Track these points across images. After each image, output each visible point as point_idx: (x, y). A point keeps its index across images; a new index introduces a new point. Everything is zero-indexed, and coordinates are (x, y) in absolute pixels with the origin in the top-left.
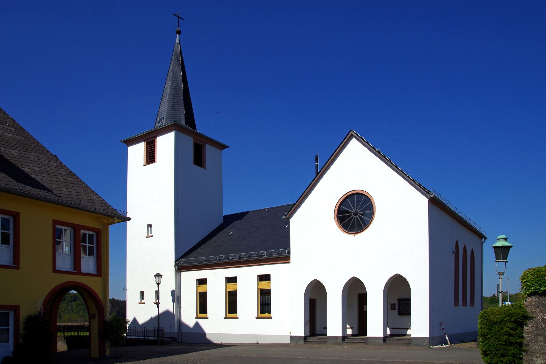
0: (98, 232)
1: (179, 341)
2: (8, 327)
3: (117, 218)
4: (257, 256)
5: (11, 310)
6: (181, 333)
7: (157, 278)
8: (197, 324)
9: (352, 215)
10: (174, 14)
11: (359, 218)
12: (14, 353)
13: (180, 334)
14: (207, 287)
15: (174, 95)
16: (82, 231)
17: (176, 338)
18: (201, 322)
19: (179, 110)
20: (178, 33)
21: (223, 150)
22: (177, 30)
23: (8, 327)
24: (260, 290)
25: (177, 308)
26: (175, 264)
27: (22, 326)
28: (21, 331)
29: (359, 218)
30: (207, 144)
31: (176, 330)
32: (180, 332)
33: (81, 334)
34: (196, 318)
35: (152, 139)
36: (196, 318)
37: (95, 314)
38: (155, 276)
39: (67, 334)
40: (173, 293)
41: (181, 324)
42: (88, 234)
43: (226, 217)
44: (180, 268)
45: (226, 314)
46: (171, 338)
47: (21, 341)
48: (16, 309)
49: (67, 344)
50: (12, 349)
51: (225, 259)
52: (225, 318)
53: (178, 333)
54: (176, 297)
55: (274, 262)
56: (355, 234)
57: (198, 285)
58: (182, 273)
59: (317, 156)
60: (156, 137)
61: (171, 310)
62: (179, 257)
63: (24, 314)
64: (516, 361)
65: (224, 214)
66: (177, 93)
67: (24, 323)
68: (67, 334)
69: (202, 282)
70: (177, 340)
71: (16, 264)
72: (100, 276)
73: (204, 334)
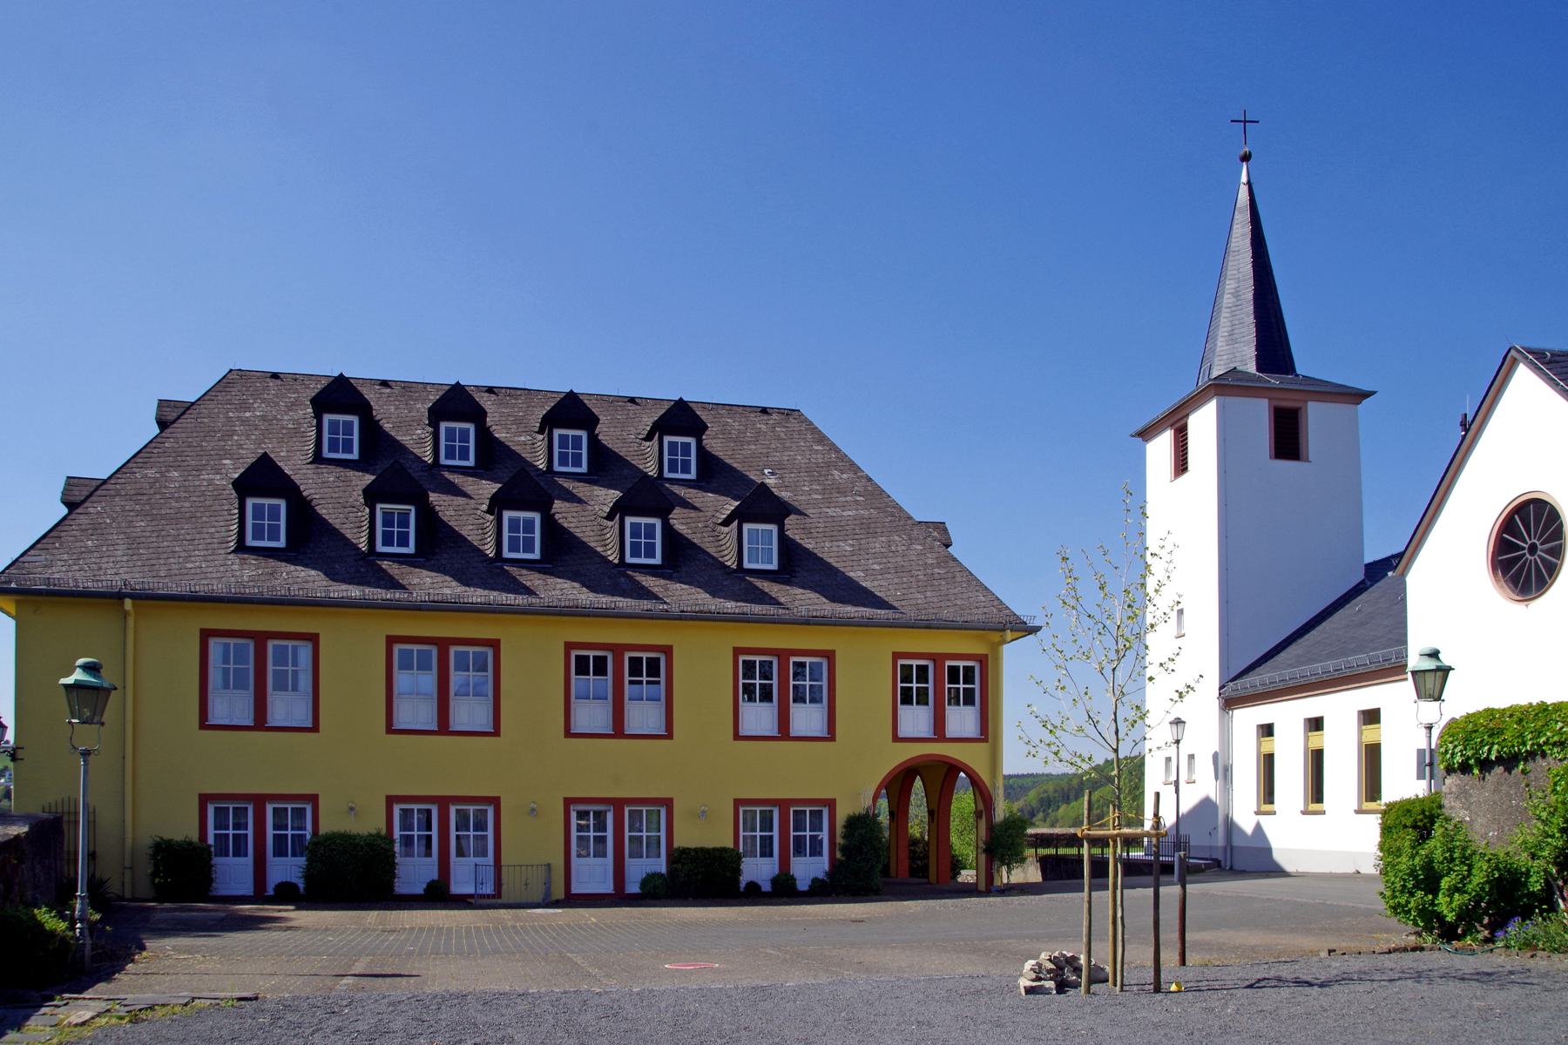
0: (982, 660)
1: (1226, 866)
2: (770, 834)
3: (1011, 631)
4: (1341, 669)
5: (825, 806)
6: (1232, 849)
7: (1174, 727)
8: (1258, 828)
9: (1524, 554)
10: (1232, 121)
11: (1538, 560)
12: (830, 874)
13: (1229, 851)
14: (1325, 736)
15: (1234, 309)
16: (949, 663)
17: (1220, 859)
18: (1263, 819)
19: (1243, 339)
20: (1246, 158)
21: (1361, 403)
22: (1242, 153)
23: (770, 834)
24: (1366, 745)
25: (1225, 791)
26: (1220, 694)
27: (839, 830)
28: (839, 840)
29: (1538, 560)
30: (1311, 400)
31: (1220, 840)
32: (1229, 847)
33: (1062, 851)
34: (1258, 813)
35: (1182, 422)
36: (1258, 813)
37: (982, 811)
38: (1171, 723)
39: (1043, 852)
40: (1215, 756)
41: (1230, 826)
42: (964, 667)
43: (1369, 567)
44: (1230, 702)
45: (1259, 806)
46: (1212, 859)
47: (838, 855)
48: (831, 804)
49: (1041, 871)
50: (826, 867)
51: (1270, 683)
52: (1304, 813)
53: (1225, 848)
54: (1223, 771)
55: (1397, 675)
56: (1526, 603)
57: (1364, 727)
58: (1235, 711)
59: (1466, 415)
60: (1187, 416)
61: (1213, 797)
62: (1232, 676)
63: (842, 815)
64: (963, 872)
65: (1368, 559)
66: (1238, 303)
67: (845, 827)
68: (1043, 852)
69: (1371, 717)
70: (1222, 864)
71: (831, 736)
72: (985, 740)
73: (1269, 850)
